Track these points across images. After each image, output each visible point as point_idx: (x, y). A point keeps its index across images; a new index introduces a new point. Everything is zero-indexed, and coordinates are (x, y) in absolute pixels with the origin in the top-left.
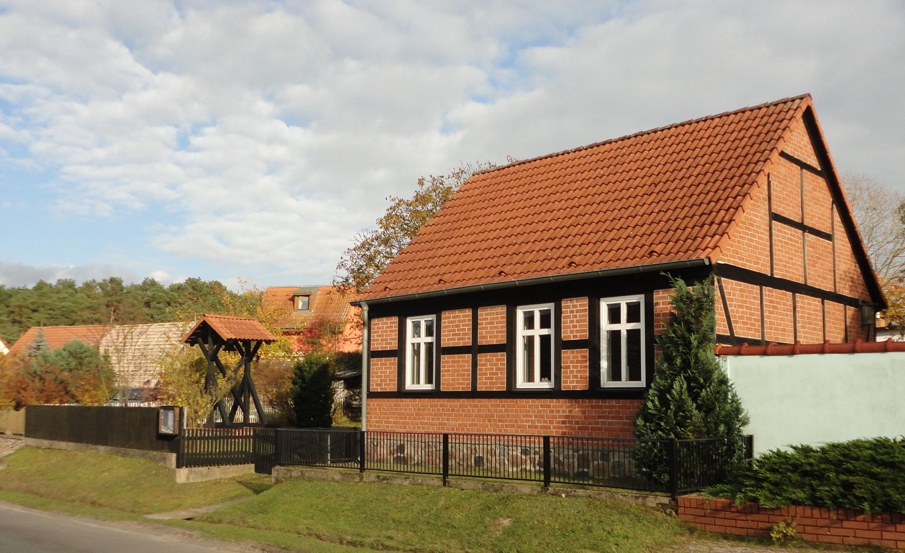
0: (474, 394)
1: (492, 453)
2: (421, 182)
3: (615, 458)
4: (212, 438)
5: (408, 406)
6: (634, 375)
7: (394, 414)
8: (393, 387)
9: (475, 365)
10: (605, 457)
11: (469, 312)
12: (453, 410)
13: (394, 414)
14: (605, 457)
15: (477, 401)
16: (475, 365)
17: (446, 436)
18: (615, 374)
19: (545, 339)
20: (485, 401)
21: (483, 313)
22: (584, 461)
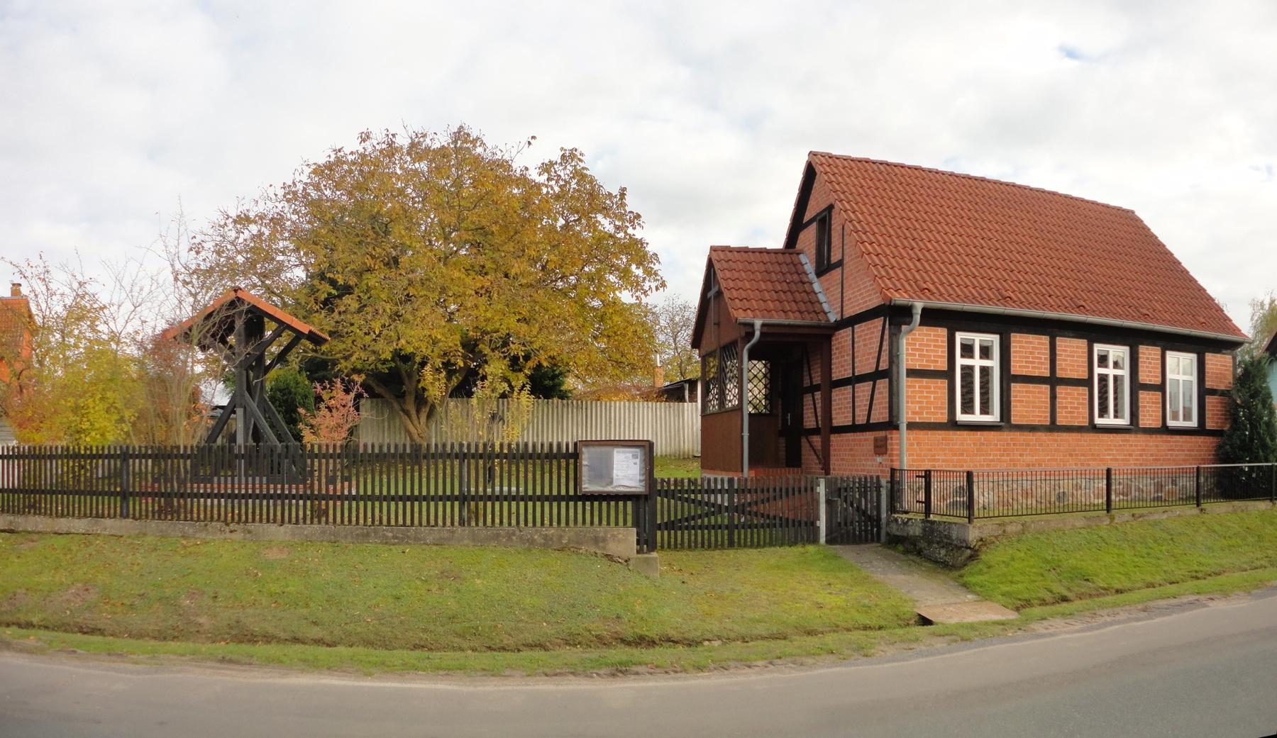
0: (1053, 427)
1: (1078, 487)
2: (365, 137)
3: (1180, 483)
4: (268, 497)
5: (965, 440)
6: (985, 409)
7: (944, 450)
8: (943, 417)
9: (1053, 397)
10: (1174, 483)
11: (1045, 340)
12: (1028, 445)
13: (944, 450)
14: (1174, 483)
15: (1056, 435)
16: (1053, 397)
17: (927, 475)
18: (967, 408)
19: (985, 371)
20: (1065, 436)
21: (1061, 342)
22: (1159, 487)
